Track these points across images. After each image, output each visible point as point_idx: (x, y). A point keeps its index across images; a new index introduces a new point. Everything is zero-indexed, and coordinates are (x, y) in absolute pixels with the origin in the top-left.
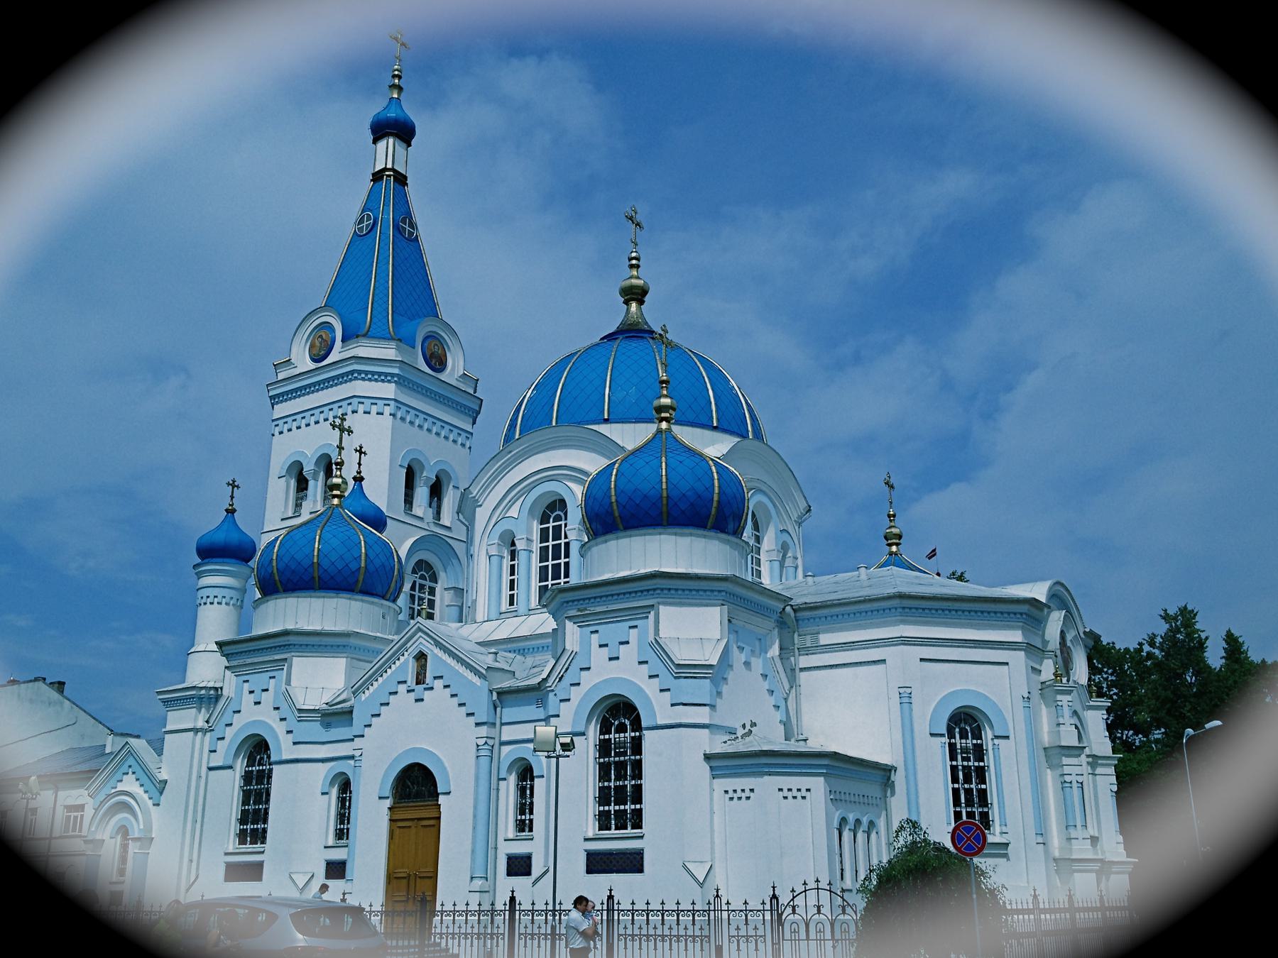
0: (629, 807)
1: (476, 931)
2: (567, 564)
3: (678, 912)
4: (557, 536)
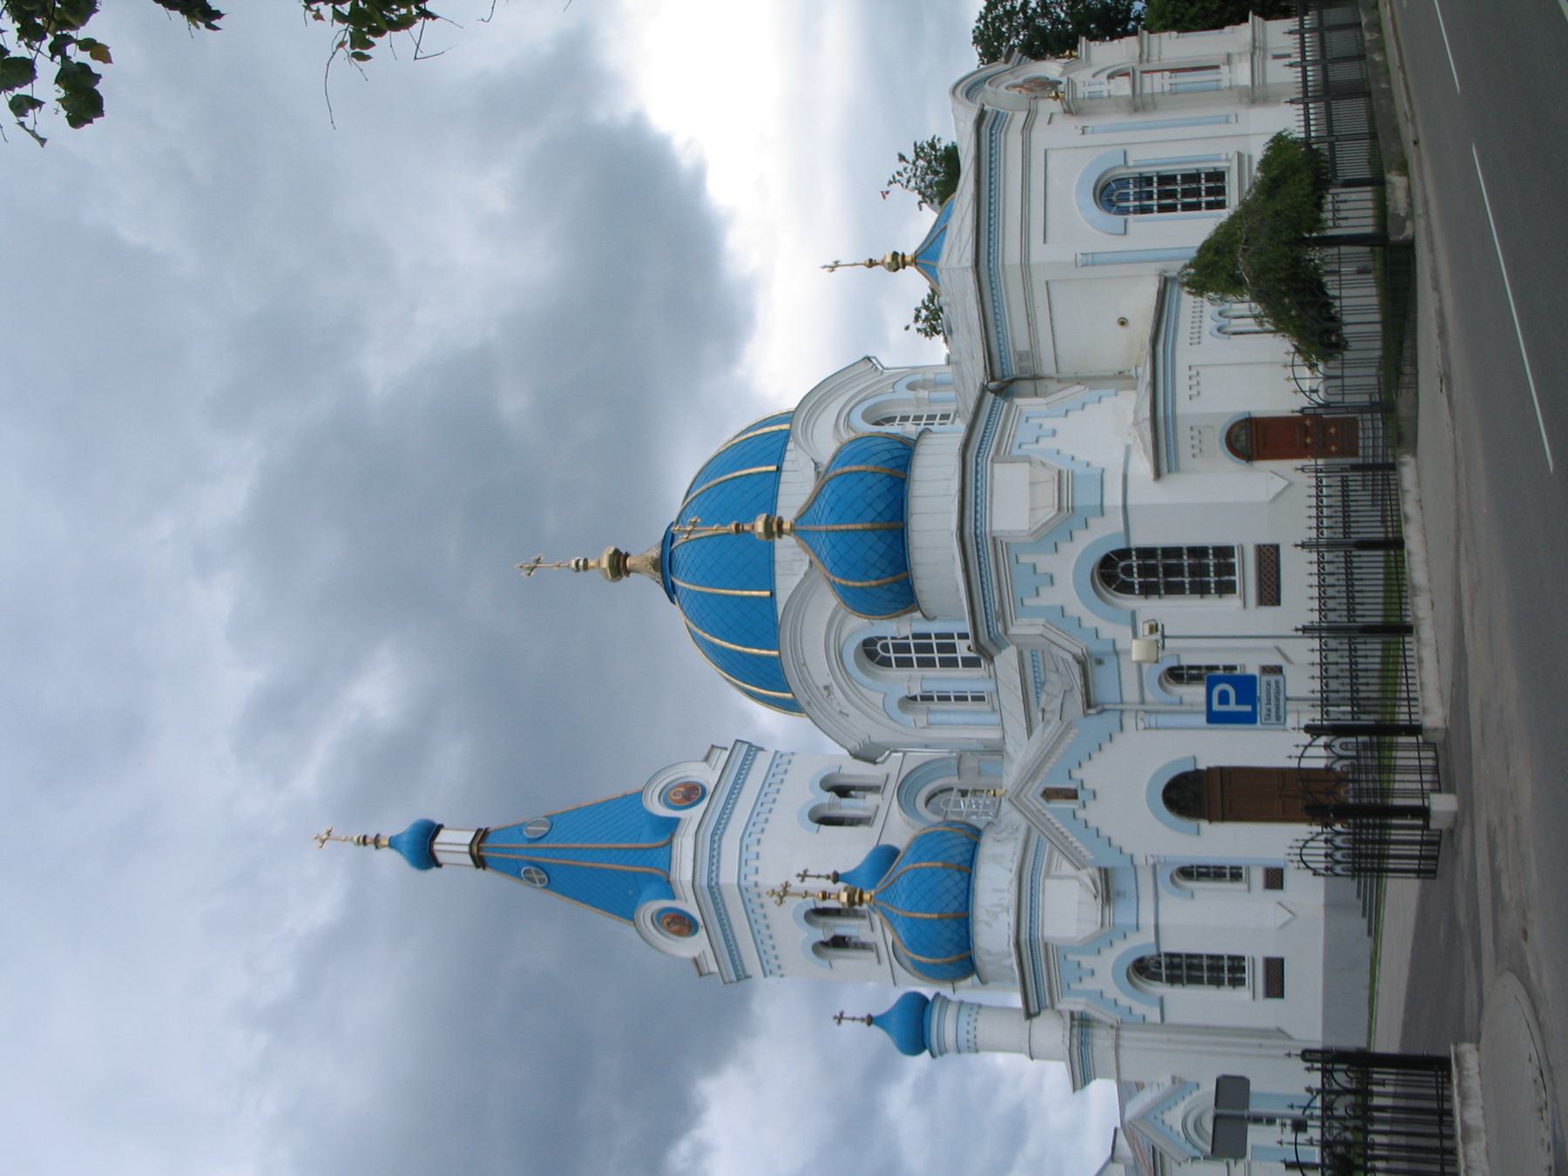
0: (1212, 579)
2: (938, 636)
4: (906, 648)
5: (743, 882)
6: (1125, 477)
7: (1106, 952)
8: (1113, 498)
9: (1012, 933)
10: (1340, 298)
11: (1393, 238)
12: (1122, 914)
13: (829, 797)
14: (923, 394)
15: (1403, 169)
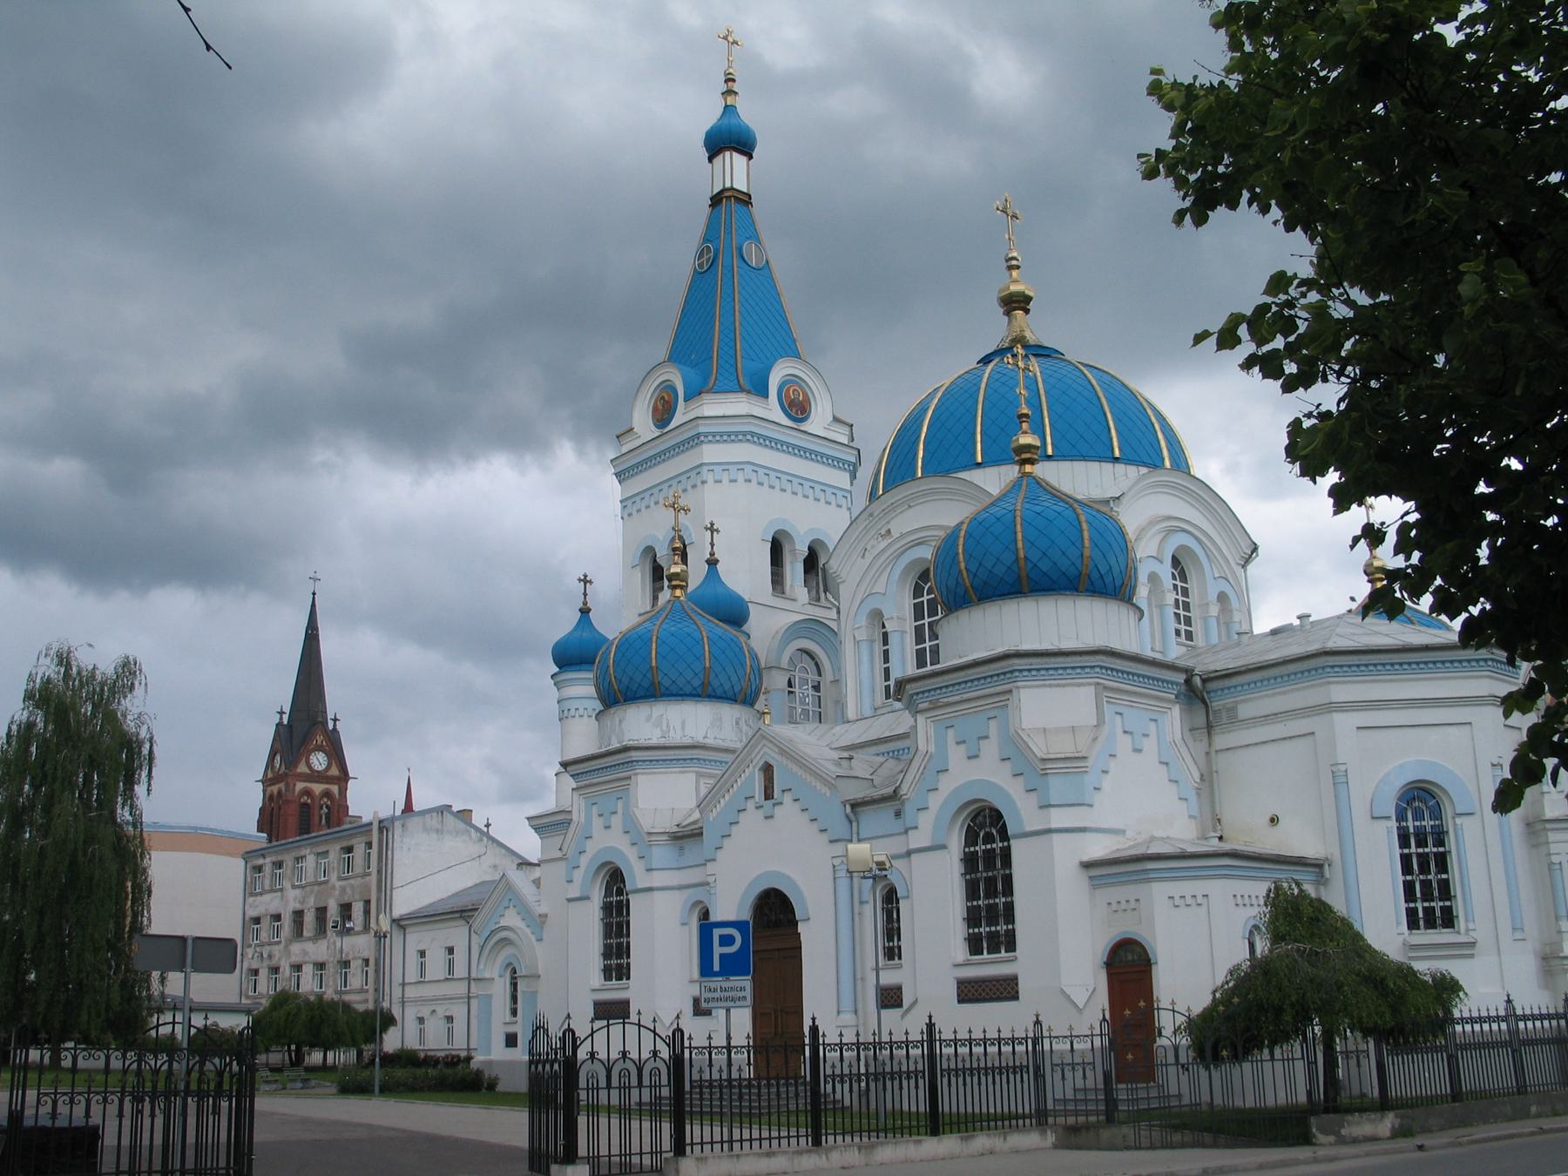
0: (984, 930)
5: (705, 469)
6: (1083, 830)
7: (626, 839)
8: (1058, 818)
9: (643, 742)
10: (1272, 1059)
11: (1313, 1120)
12: (662, 854)
13: (803, 551)
14: (1214, 610)
15: (1400, 1133)
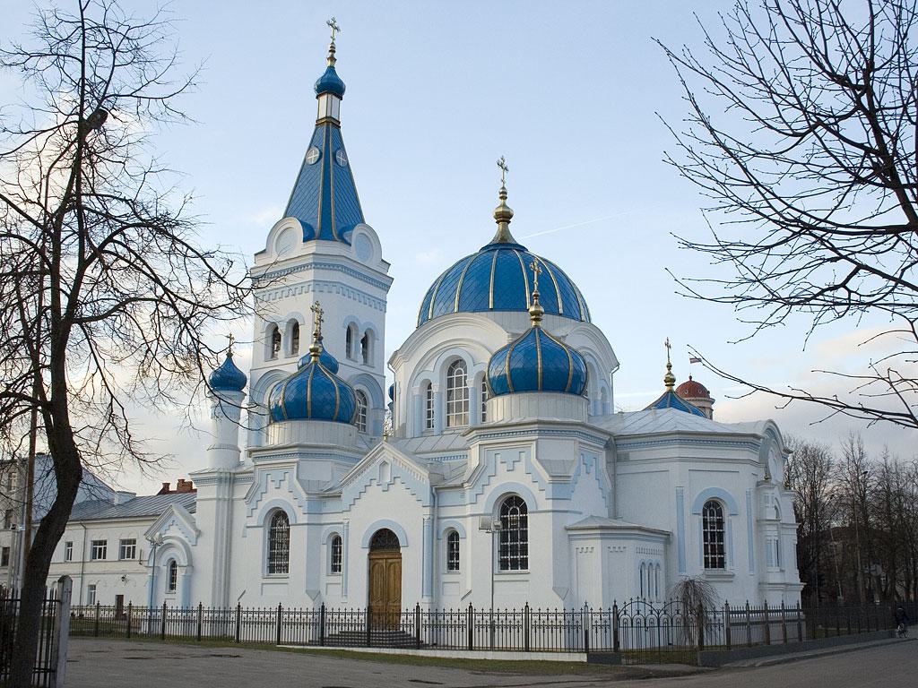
1: (563, 624)
3: (259, 612)
4: (459, 384)
6: (566, 512)
